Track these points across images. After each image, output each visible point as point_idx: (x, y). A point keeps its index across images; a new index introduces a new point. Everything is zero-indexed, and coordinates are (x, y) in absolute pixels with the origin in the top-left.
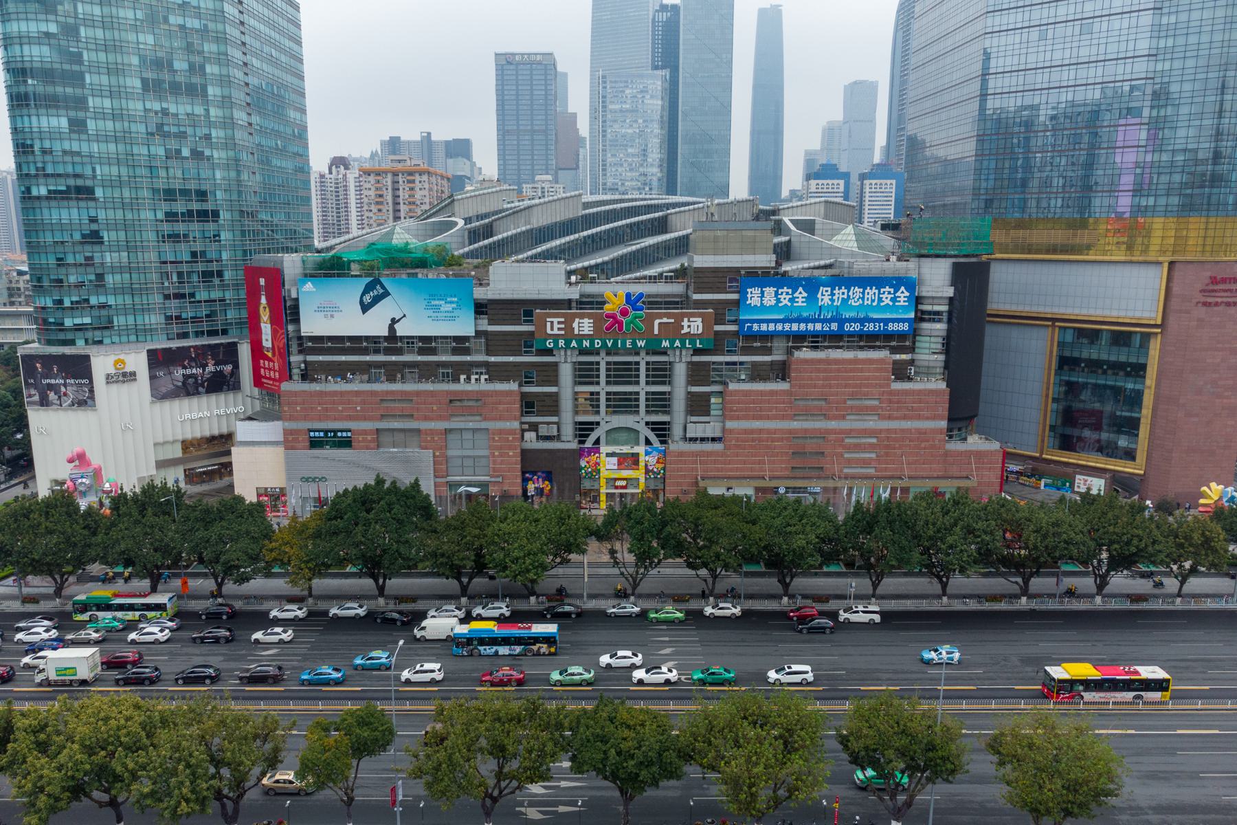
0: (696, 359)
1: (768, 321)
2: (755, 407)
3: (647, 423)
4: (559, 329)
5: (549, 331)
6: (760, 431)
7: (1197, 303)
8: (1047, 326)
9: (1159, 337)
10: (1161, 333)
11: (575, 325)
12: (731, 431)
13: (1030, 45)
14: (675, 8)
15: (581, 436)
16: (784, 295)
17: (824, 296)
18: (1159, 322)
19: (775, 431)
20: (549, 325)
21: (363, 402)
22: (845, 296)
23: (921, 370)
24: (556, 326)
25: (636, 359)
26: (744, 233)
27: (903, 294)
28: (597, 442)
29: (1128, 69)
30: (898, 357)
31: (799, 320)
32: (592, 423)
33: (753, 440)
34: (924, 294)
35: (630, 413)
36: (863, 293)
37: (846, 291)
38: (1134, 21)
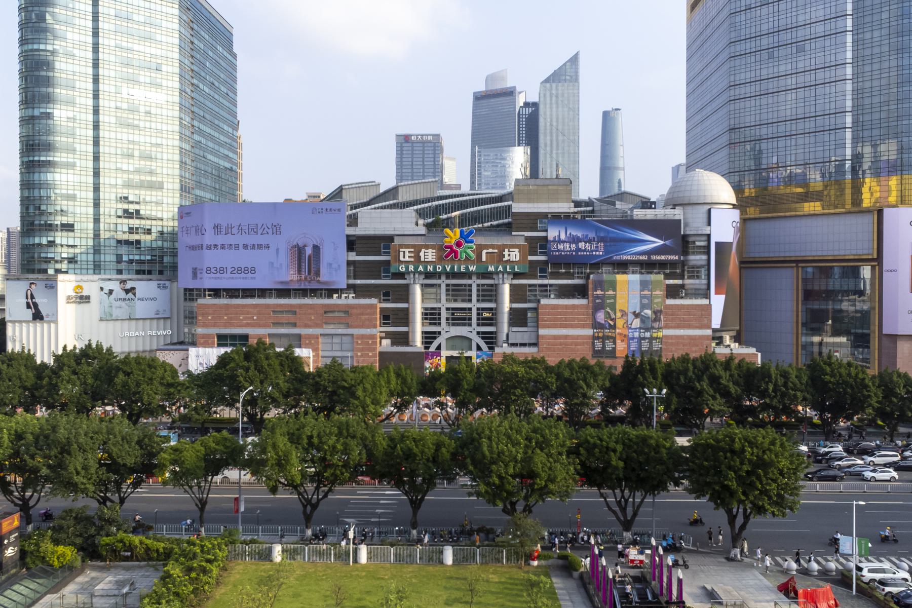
0: (516, 282)
2: (563, 319)
3: (478, 333)
4: (409, 257)
6: (566, 337)
11: (422, 254)
12: (543, 337)
13: (762, 63)
14: (535, 105)
15: (426, 343)
18: (875, 256)
19: (578, 337)
20: (401, 254)
21: (259, 313)
23: (689, 292)
24: (407, 254)
25: (469, 282)
26: (550, 187)
28: (439, 348)
29: (833, 74)
30: (671, 282)
32: (434, 333)
33: (561, 344)
34: (688, 233)
35: (464, 325)
38: (833, 41)
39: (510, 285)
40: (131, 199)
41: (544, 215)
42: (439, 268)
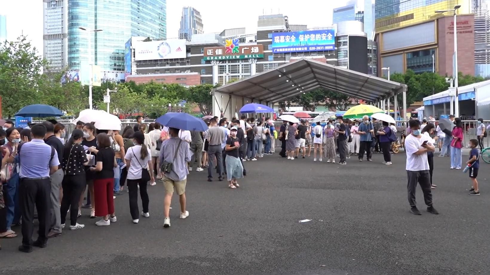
0: (258, 63)
1: (282, 48)
4: (211, 53)
5: (208, 54)
7: (448, 33)
8: (402, 54)
9: (438, 49)
10: (438, 47)
16: (287, 38)
17: (301, 37)
18: (436, 43)
20: (208, 52)
22: (309, 38)
27: (330, 35)
31: (293, 47)
34: (338, 35)
36: (315, 36)
37: (309, 36)
39: (256, 64)
40: (361, 100)
41: (270, 32)
42: (224, 58)
